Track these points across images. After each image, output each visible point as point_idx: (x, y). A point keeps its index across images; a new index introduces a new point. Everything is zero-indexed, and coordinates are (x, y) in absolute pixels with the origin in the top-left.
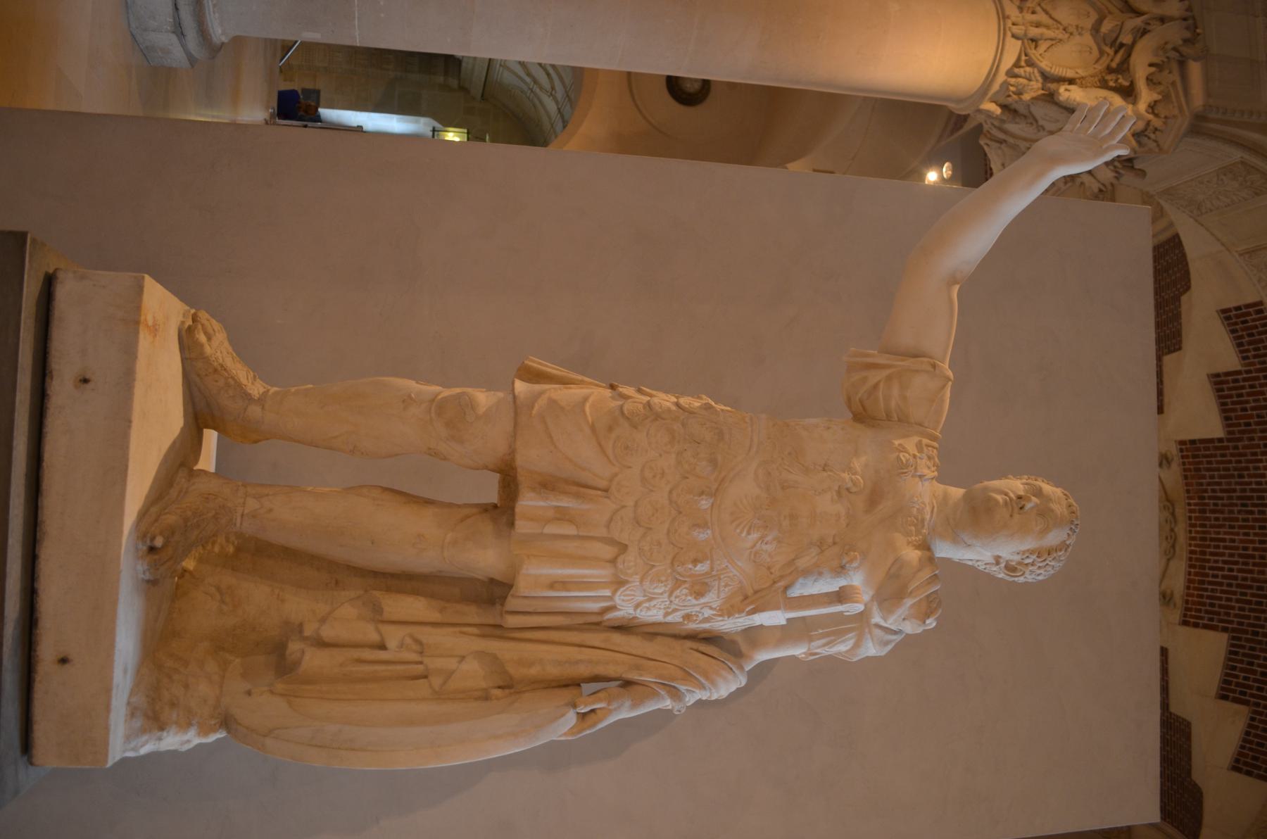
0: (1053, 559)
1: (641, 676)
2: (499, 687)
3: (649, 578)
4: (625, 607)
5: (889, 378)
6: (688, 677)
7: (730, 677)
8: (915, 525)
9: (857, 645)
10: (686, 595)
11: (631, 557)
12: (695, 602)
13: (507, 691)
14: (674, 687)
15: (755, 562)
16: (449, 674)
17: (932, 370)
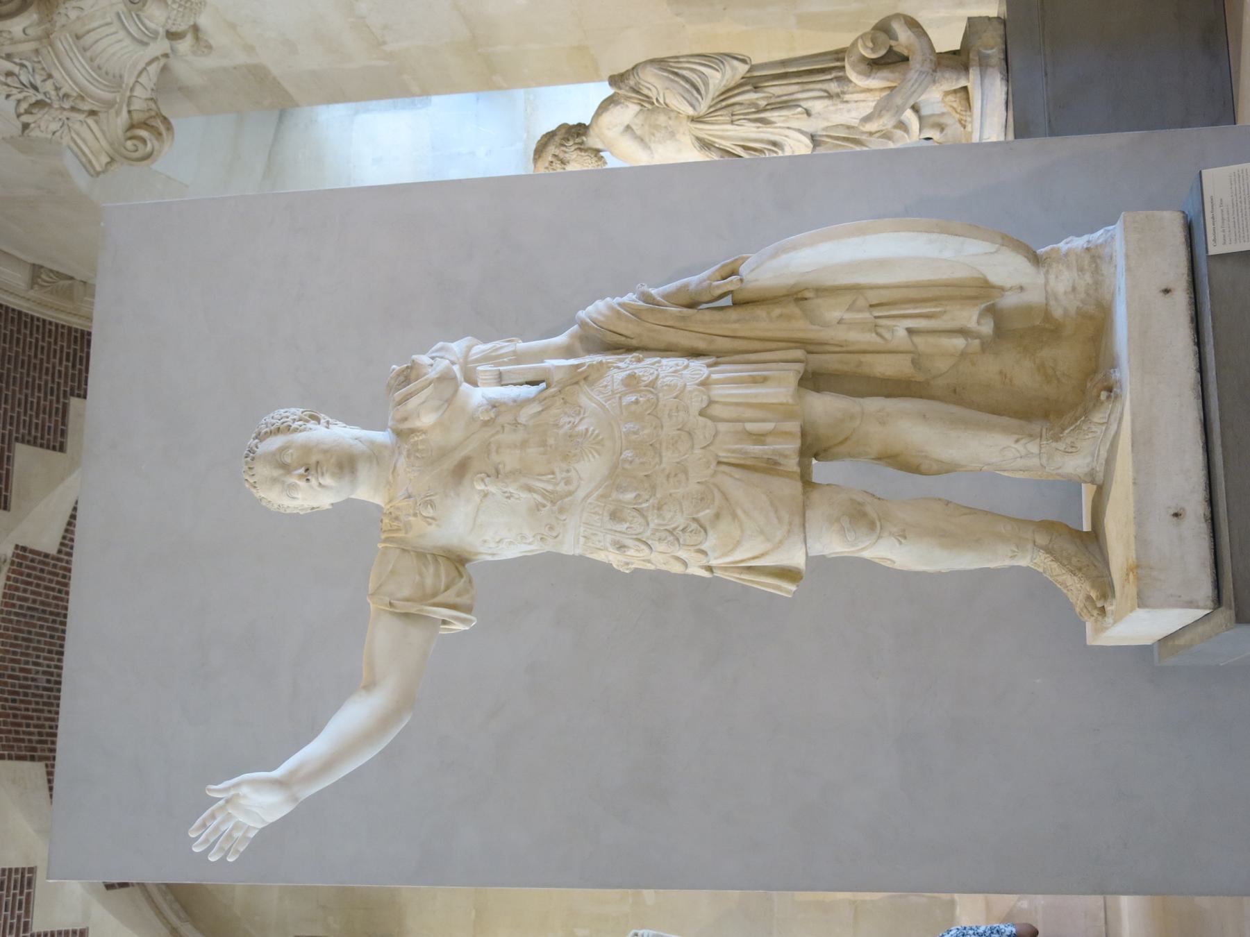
0: (274, 424)
1: (680, 312)
2: (806, 299)
3: (678, 388)
4: (698, 368)
5: (435, 595)
6: (636, 313)
7: (595, 316)
8: (418, 451)
9: (469, 348)
10: (644, 376)
11: (696, 405)
12: (636, 371)
13: (799, 296)
14: (647, 303)
15: (580, 407)
16: (851, 308)
17: (392, 601)
